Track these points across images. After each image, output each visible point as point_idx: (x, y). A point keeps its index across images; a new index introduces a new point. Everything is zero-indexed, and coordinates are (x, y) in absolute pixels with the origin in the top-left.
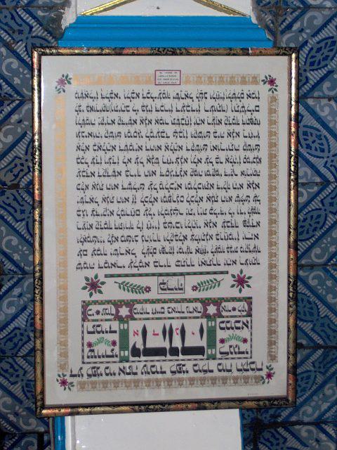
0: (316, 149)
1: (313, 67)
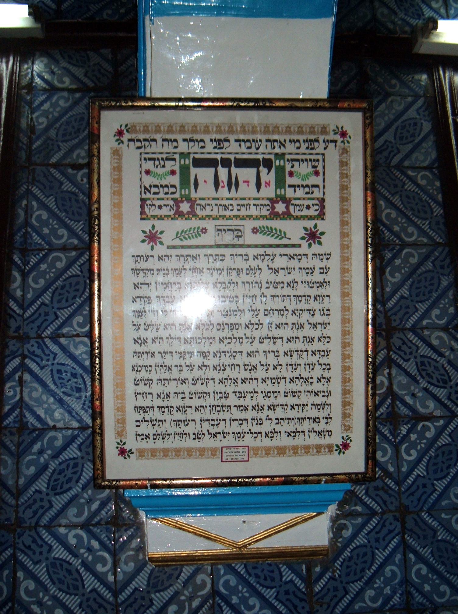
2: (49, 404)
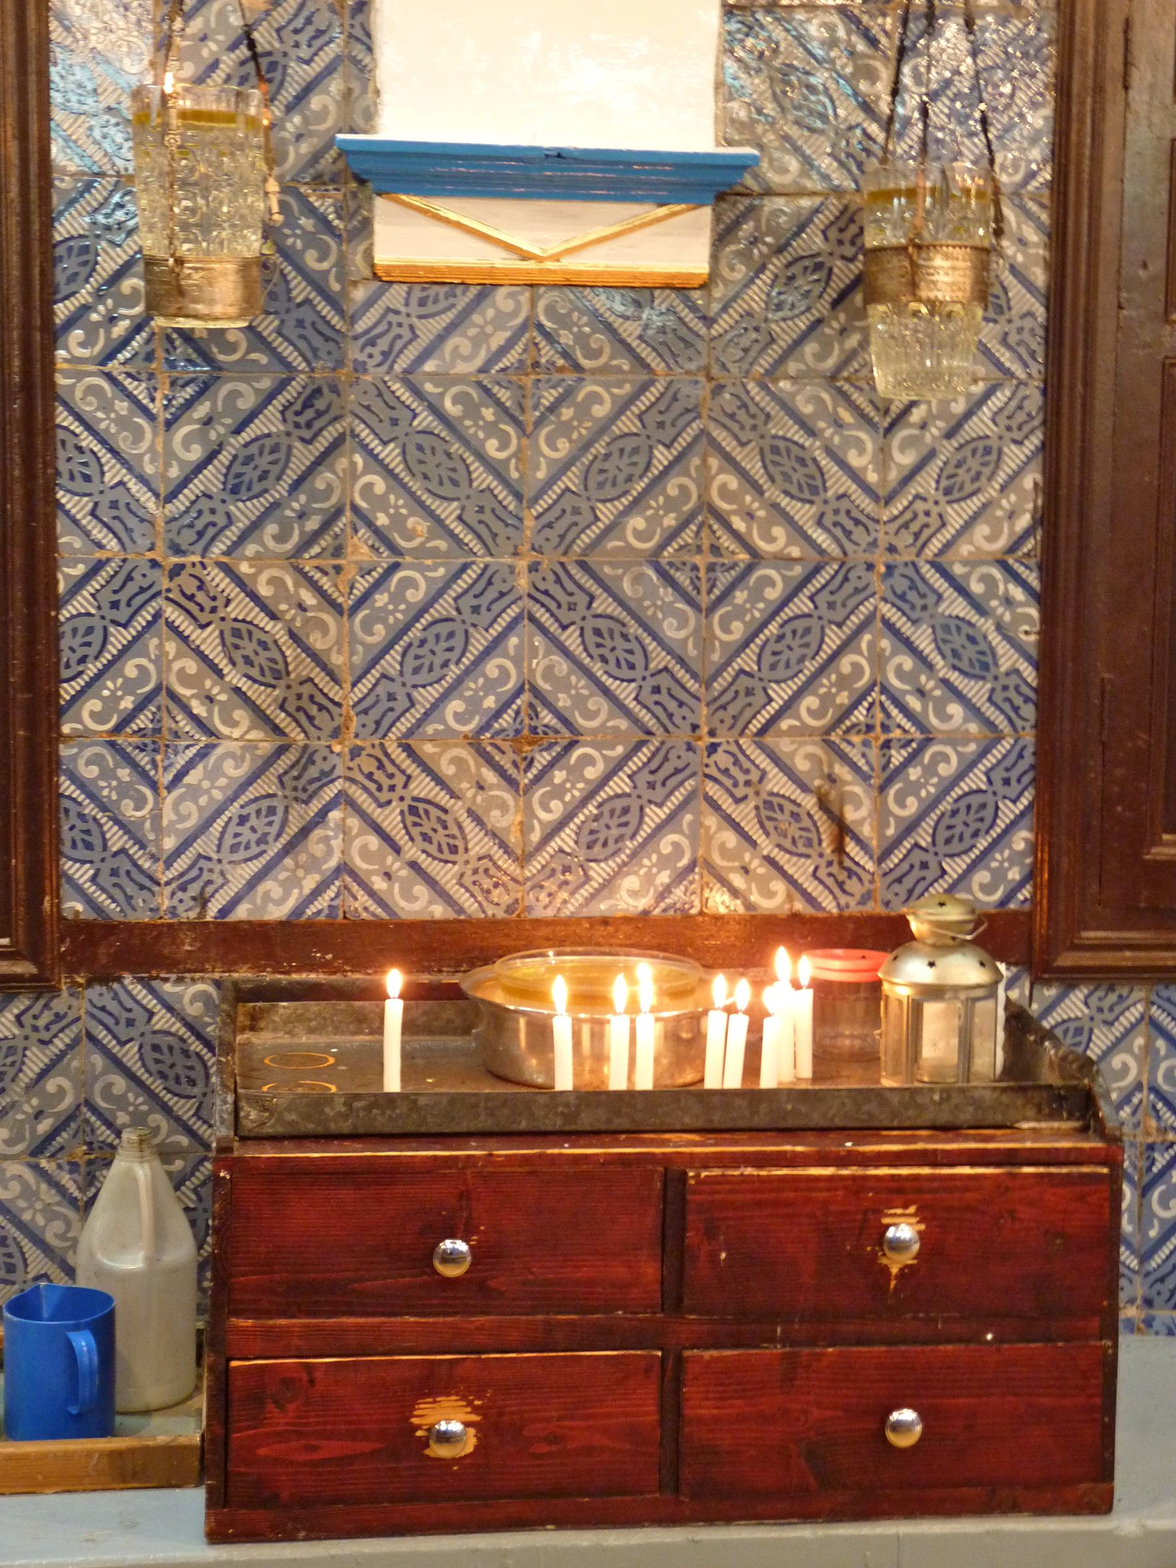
0: (237, 835)
1: (939, 630)
2: (487, 323)
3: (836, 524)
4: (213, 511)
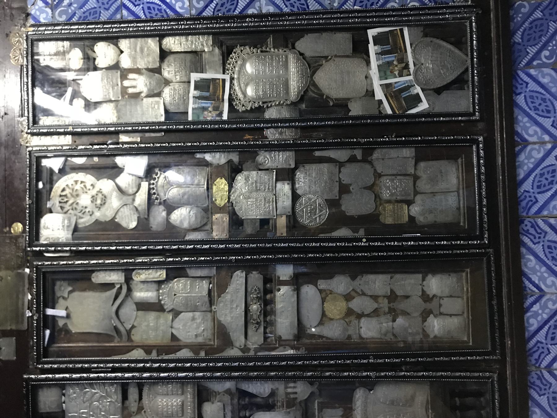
0: (537, 97)
1: (94, 10)
3: (546, 385)
4: (543, 348)
